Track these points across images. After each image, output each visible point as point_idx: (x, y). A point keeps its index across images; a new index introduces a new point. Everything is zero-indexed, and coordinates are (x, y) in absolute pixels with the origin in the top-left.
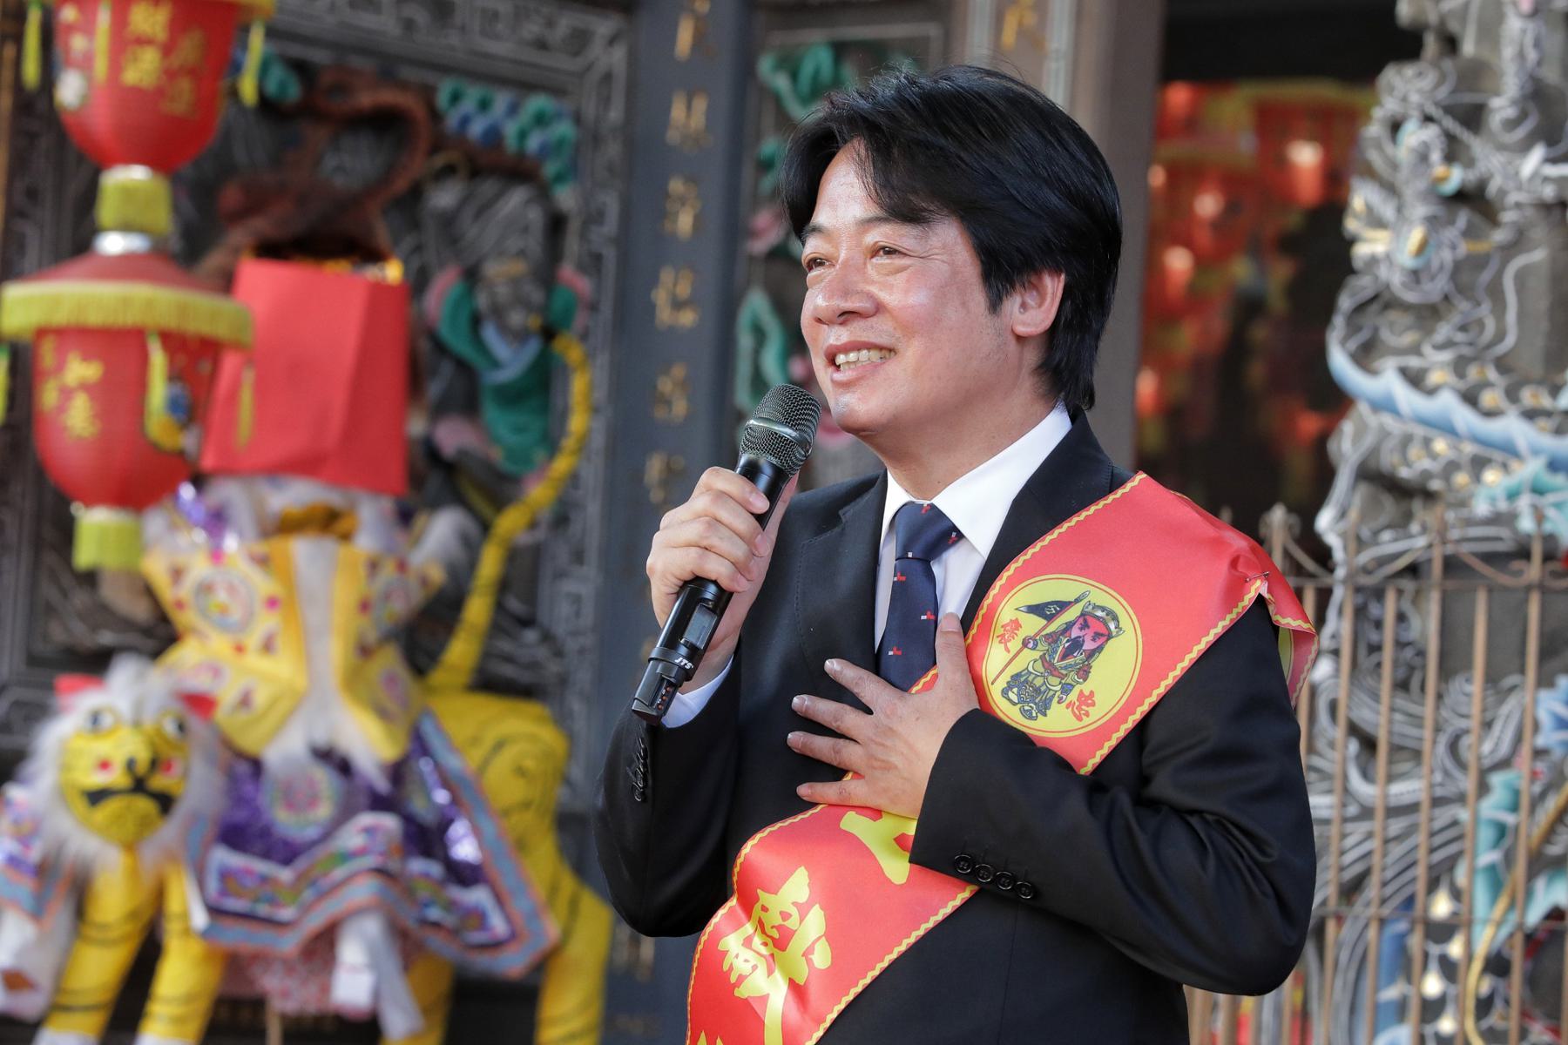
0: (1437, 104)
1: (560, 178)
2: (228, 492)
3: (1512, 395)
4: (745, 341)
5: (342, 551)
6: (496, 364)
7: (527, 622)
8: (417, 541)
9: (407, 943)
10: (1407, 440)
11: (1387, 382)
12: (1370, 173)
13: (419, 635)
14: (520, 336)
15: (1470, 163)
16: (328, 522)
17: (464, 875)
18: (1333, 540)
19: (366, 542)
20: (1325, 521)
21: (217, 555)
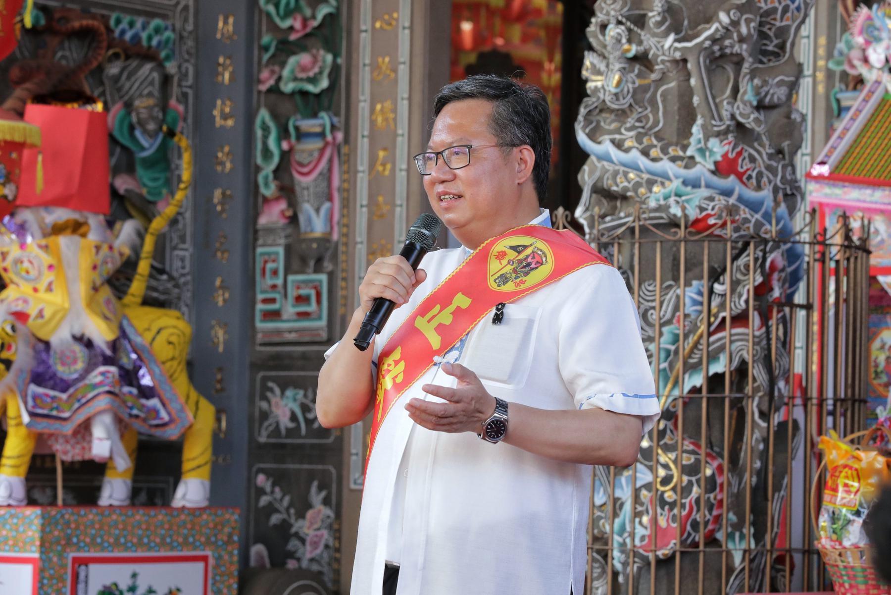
0: (621, 15)
1: (168, 58)
2: (26, 215)
3: (664, 151)
4: (259, 133)
5: (82, 241)
6: (143, 149)
7: (162, 271)
8: (117, 236)
9: (121, 425)
10: (616, 173)
11: (606, 146)
12: (591, 48)
13: (118, 280)
14: (152, 135)
15: (640, 43)
16: (77, 228)
17: (146, 393)
18: (582, 221)
19: (93, 237)
20: (579, 212)
21: (23, 246)
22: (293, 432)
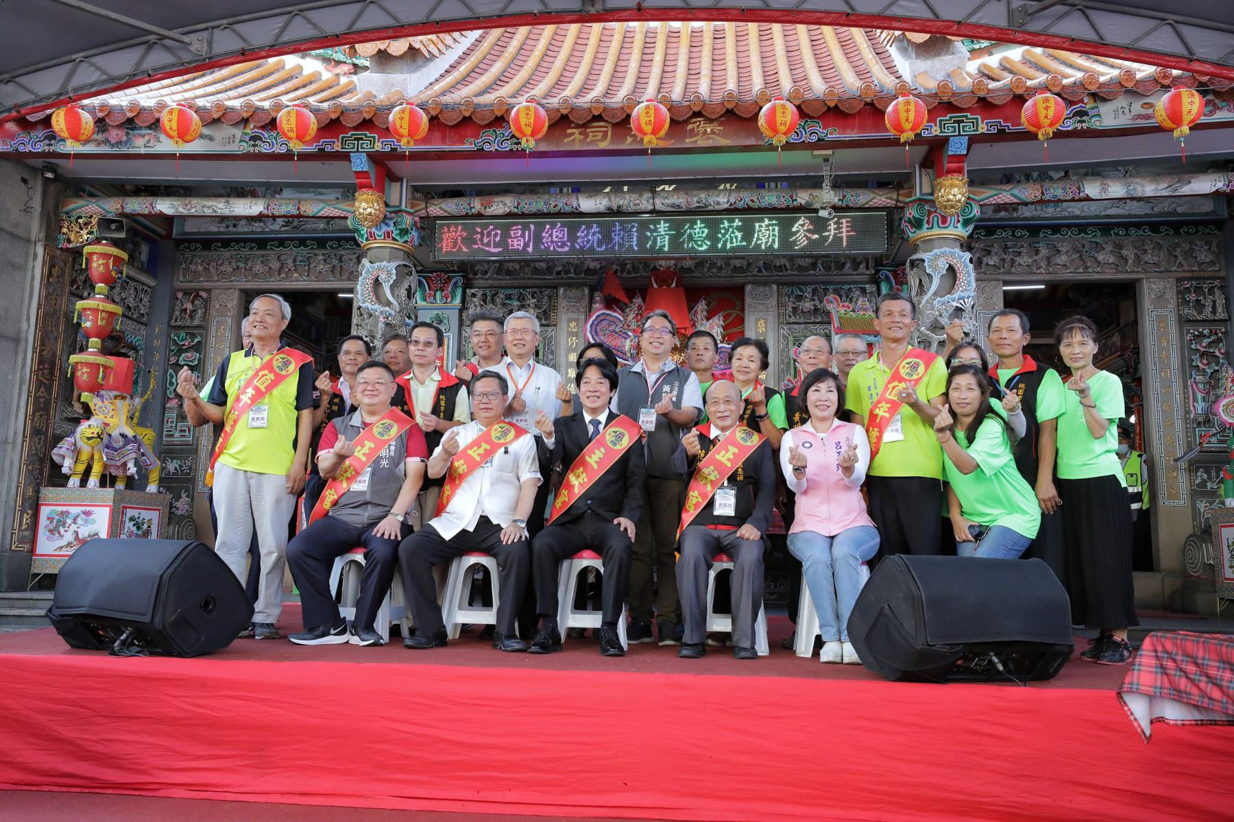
16: (123, 398)
22: (176, 474)
